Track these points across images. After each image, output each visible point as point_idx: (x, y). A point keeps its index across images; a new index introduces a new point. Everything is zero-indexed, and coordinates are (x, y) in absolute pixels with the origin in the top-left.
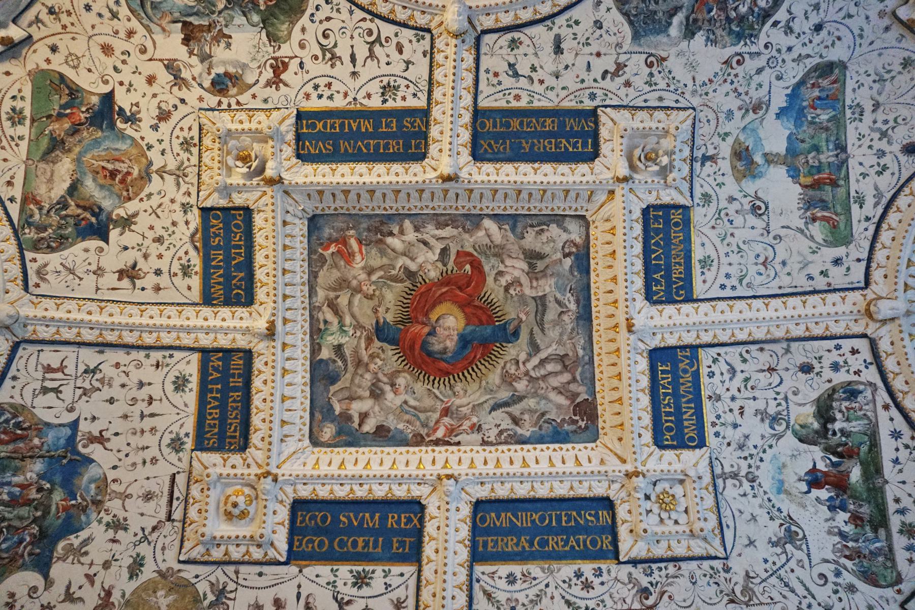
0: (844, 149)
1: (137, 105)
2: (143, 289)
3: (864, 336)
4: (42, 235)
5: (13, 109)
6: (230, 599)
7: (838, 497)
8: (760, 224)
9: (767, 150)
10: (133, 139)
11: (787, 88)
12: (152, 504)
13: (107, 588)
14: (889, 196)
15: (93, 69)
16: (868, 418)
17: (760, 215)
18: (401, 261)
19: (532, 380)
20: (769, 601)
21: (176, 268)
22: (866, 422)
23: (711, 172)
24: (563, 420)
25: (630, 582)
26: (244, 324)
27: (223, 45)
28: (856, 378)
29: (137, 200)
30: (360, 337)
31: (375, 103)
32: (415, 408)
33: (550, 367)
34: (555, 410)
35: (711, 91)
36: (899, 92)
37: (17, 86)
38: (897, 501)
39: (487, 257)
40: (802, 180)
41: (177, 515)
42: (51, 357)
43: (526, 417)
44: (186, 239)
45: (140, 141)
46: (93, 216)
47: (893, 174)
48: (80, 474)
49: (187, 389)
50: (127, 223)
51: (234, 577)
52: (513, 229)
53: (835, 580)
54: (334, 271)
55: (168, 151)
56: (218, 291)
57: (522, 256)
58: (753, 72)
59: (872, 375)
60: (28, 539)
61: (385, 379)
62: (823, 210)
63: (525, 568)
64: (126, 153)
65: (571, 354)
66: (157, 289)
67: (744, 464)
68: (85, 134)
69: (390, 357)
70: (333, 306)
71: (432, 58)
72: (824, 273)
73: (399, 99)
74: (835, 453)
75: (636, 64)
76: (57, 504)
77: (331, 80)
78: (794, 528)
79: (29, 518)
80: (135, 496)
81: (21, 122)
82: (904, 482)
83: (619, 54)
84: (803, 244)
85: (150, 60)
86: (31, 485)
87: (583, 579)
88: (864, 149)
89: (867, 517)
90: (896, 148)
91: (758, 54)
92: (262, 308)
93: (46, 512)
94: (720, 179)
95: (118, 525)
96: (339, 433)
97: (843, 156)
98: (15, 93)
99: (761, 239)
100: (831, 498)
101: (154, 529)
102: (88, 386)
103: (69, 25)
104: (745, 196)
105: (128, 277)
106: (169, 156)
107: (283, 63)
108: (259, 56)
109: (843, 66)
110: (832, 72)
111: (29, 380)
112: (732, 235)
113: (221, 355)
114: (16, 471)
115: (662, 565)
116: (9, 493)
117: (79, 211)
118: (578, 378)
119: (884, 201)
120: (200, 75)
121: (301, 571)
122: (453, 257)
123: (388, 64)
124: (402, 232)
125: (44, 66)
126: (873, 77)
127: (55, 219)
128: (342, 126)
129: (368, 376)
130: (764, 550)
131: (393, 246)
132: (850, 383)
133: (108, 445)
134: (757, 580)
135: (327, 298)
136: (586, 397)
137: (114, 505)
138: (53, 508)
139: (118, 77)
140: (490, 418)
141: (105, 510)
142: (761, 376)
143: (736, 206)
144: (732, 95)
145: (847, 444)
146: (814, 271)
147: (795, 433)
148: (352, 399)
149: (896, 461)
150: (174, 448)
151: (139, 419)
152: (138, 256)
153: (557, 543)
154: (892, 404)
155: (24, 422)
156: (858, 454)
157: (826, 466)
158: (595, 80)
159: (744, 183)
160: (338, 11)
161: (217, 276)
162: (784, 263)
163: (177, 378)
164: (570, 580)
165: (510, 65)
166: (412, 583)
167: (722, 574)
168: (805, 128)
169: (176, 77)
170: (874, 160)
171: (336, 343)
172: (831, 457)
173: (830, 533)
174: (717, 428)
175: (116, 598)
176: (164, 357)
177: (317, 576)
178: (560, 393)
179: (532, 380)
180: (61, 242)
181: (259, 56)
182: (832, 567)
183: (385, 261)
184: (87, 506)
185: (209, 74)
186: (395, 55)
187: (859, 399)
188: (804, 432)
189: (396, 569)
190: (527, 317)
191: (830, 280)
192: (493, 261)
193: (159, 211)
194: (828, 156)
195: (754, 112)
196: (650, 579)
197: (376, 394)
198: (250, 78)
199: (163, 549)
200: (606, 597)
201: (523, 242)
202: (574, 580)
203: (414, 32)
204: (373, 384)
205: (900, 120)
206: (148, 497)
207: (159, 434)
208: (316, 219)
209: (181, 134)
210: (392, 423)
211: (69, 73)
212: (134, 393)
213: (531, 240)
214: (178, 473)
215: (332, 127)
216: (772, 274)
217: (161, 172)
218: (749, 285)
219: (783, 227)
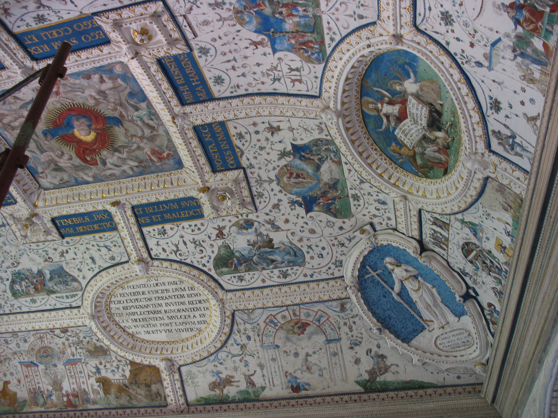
1: (292, 209)
4: (326, 147)
5: (358, 201)
10: (291, 194)
15: (319, 222)
18: (125, 155)
21: (247, 137)
29: (281, 166)
30: (128, 116)
31: (167, 226)
37: (359, 210)
45: (286, 193)
48: (259, 24)
49: (213, 78)
50: (283, 154)
52: (76, 179)
54: (159, 144)
55: (270, 191)
64: (293, 187)
66: (255, 124)
68: (319, 193)
69: (106, 109)
73: (156, 230)
75: (56, 258)
85: (288, 230)
98: (359, 207)
101: (191, 9)
102: (274, 71)
103: (333, 240)
105: (274, 128)
106: (269, 189)
107: (219, 237)
114: (298, 24)
116: (298, 11)
117: (312, 157)
120: (260, 227)
122: (99, 162)
124: (132, 168)
125: (345, 220)
128: (180, 215)
133: (250, 41)
135: (157, 131)
138: (267, 3)
139: (305, 220)
141: (231, 10)
150: (205, 49)
151: (236, 58)
152: (271, 139)
160: (198, 262)
163: (222, 83)
165: (110, 250)
171: (140, 111)
177: (69, 13)
181: (232, 238)
183: (134, 154)
185: (256, 228)
186: (165, 247)
193: (266, 162)
198: (234, 229)
203: (160, 258)
204: (107, 97)
210: (85, 82)
215: (185, 214)
217: (271, 181)
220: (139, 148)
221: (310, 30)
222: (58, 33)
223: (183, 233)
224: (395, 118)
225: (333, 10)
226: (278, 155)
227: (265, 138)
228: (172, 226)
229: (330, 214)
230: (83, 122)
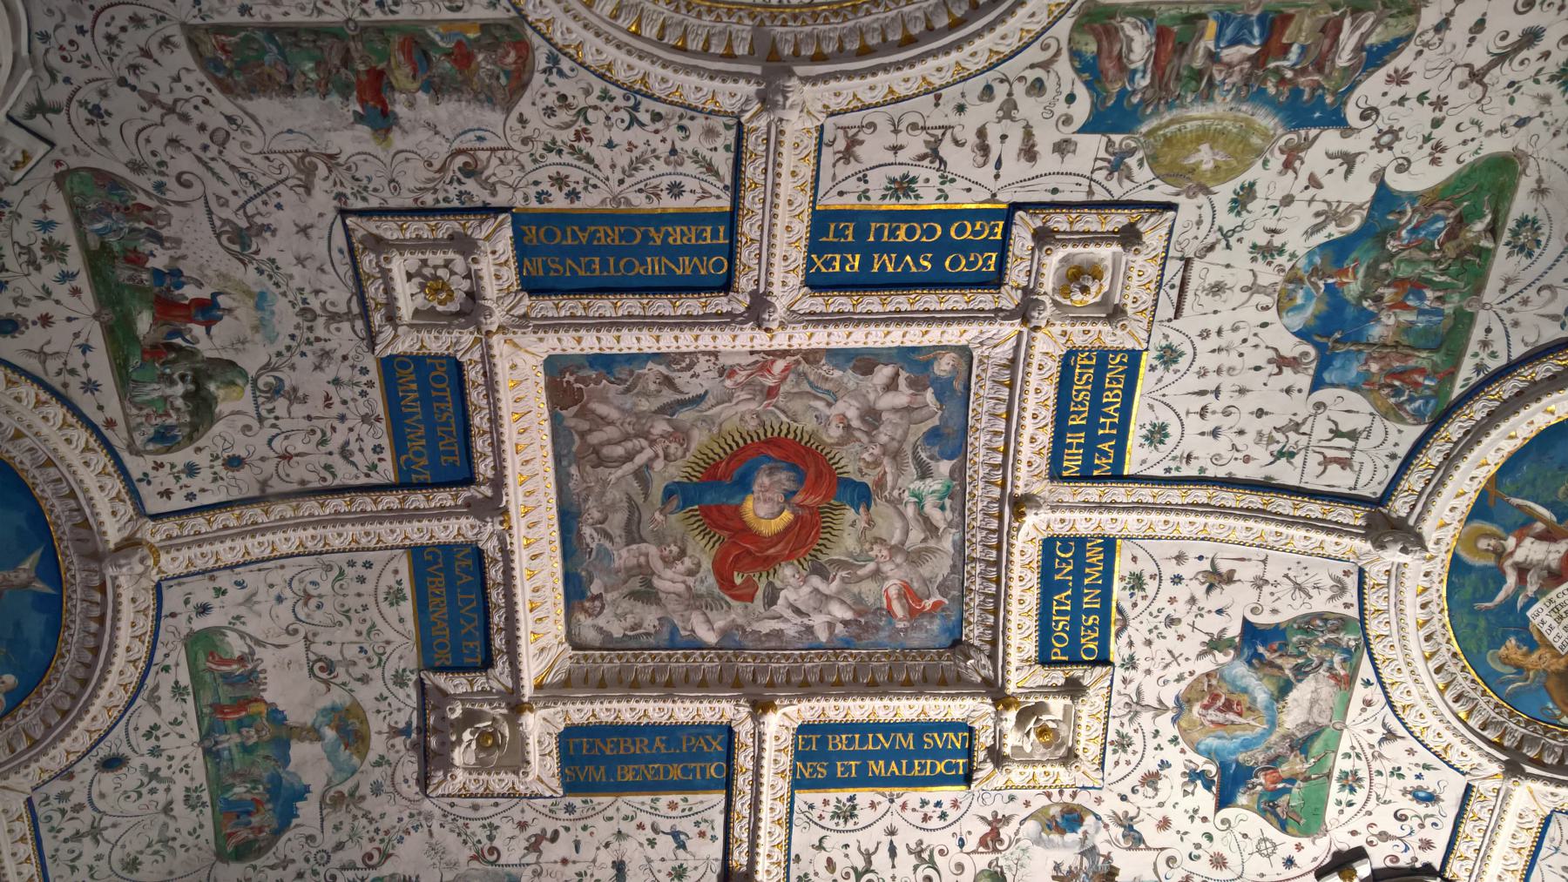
0: (207, 752)
1: (1186, 793)
2: (1201, 558)
3: (156, 517)
4: (1333, 636)
5: (1352, 790)
6: (1103, 159)
7: (168, 289)
8: (320, 648)
9: (318, 746)
10: (1197, 751)
11: (297, 826)
12: (1212, 279)
13: (1290, 172)
14: (139, 701)
15: (1240, 837)
16: (135, 405)
17: (320, 660)
19: (645, 435)
20: (272, 156)
21: (1151, 585)
22: (137, 399)
23: (396, 716)
24: (597, 382)
25: (493, 185)
26: (1058, 515)
27: (1065, 868)
28: (160, 459)
30: (893, 488)
31: (864, 796)
32: (817, 398)
33: (619, 451)
34: (610, 395)
35: (406, 819)
36: (139, 829)
37: (1343, 818)
38: (76, 292)
39: (711, 594)
40: (262, 708)
41: (1174, 267)
42: (1340, 480)
43: (653, 387)
44: (1133, 624)
45: (1187, 748)
46: (1261, 655)
47: (136, 729)
49: (1149, 427)
50: (1215, 644)
51: (1095, 187)
52: (674, 630)
53: (164, 179)
55: (1149, 736)
56: (1095, 556)
57: (662, 595)
58: (349, 844)
59: (136, 466)
60: (1404, 233)
61: (858, 434)
62: (230, 674)
63: (655, 204)
64: (1208, 734)
65: (588, 468)
67: (320, 331)
68: (1261, 758)
69: (850, 464)
70: (931, 529)
71: (789, 854)
72: (221, 592)
73: (833, 802)
74: (179, 349)
76: (1355, 278)
77: (924, 825)
78: (237, 248)
79: (1401, 261)
80: (1237, 289)
81: (1344, 775)
82: (69, 319)
83: (537, 863)
84: (253, 627)
86: (1391, 307)
87: (566, 190)
88: (178, 755)
89: (120, 263)
90: (136, 762)
91: (343, 868)
92: (1033, 534)
93: (1372, 270)
94: (383, 706)
95: (1266, 252)
96: (928, 365)
97: (207, 743)
99: (319, 629)
100: (180, 286)
101: (1211, 248)
102: (1293, 436)
104: (344, 684)
105: (1220, 575)
106: (1149, 728)
107: (986, 846)
108: (1018, 853)
109: (221, 856)
110: (236, 847)
111: (1373, 452)
112: (359, 634)
113: (1096, 473)
115: (443, 205)
117: (1279, 661)
118: (576, 437)
119: (145, 693)
120: (1097, 831)
121: (994, 195)
122: (760, 594)
123: (847, 846)
125: (1305, 841)
126: (176, 845)
127: (1314, 654)
128: (910, 767)
129: (883, 439)
130: (283, 220)
131: (844, 607)
132: (168, 450)
133: (1272, 354)
134: (291, 182)
135: (939, 538)
136: (564, 412)
137: (1269, 275)
138: (1361, 272)
139: (1208, 827)
140: (707, 386)
142: (301, 448)
143: (357, 671)
144: (375, 815)
145: (163, 364)
146: (235, 594)
147: (243, 373)
148: (908, 409)
149: (85, 348)
152: (1202, 601)
153: (607, 235)
154: (103, 429)
155: (1388, 395)
156: (144, 352)
157: (190, 331)
158: (567, 829)
159: (348, 701)
161: (1093, 575)
162: (280, 599)
163: (1161, 442)
164: (586, 189)
166: (825, 183)
167: (348, 192)
168: (265, 775)
169: (1131, 828)
170: (164, 743)
171: (928, 481)
172: (184, 344)
173: (178, 242)
174: (364, 379)
175: (1277, 160)
176: (1178, 469)
177: (969, 190)
178: (602, 418)
179: (645, 435)
180: (1308, 624)
181: (1018, 853)
182: (169, 196)
183: (855, 589)
184: (1311, 275)
185: (1085, 833)
186: (838, 856)
187: (152, 431)
188: (229, 376)
189: (850, 202)
190: (654, 516)
191: (212, 585)
192: (702, 589)
193: (1169, 658)
194: (229, 741)
195: (341, 794)
196: (463, 188)
197: (872, 417)
198: (1032, 827)
199: (1199, 223)
200: (529, 166)
201: (660, 613)
202: (579, 188)
204: (876, 428)
205: (134, 796)
206: (1217, 289)
207: (1195, 368)
208: (949, 643)
209: (1129, 756)
210: (850, 378)
211: (1273, 833)
212: (1226, 423)
213: (650, 617)
214: (1170, 320)
216: (295, 584)
217: (1161, 708)
218: (329, 568)
219: (285, 646)
220: (877, 575)
221: (1430, 344)
222: (910, 232)
223: (897, 822)
224: (1545, 573)
225: (1514, 303)
226: (1203, 643)
227: (1188, 597)
228: (877, 798)
229: (1272, 818)
230: (779, 481)
